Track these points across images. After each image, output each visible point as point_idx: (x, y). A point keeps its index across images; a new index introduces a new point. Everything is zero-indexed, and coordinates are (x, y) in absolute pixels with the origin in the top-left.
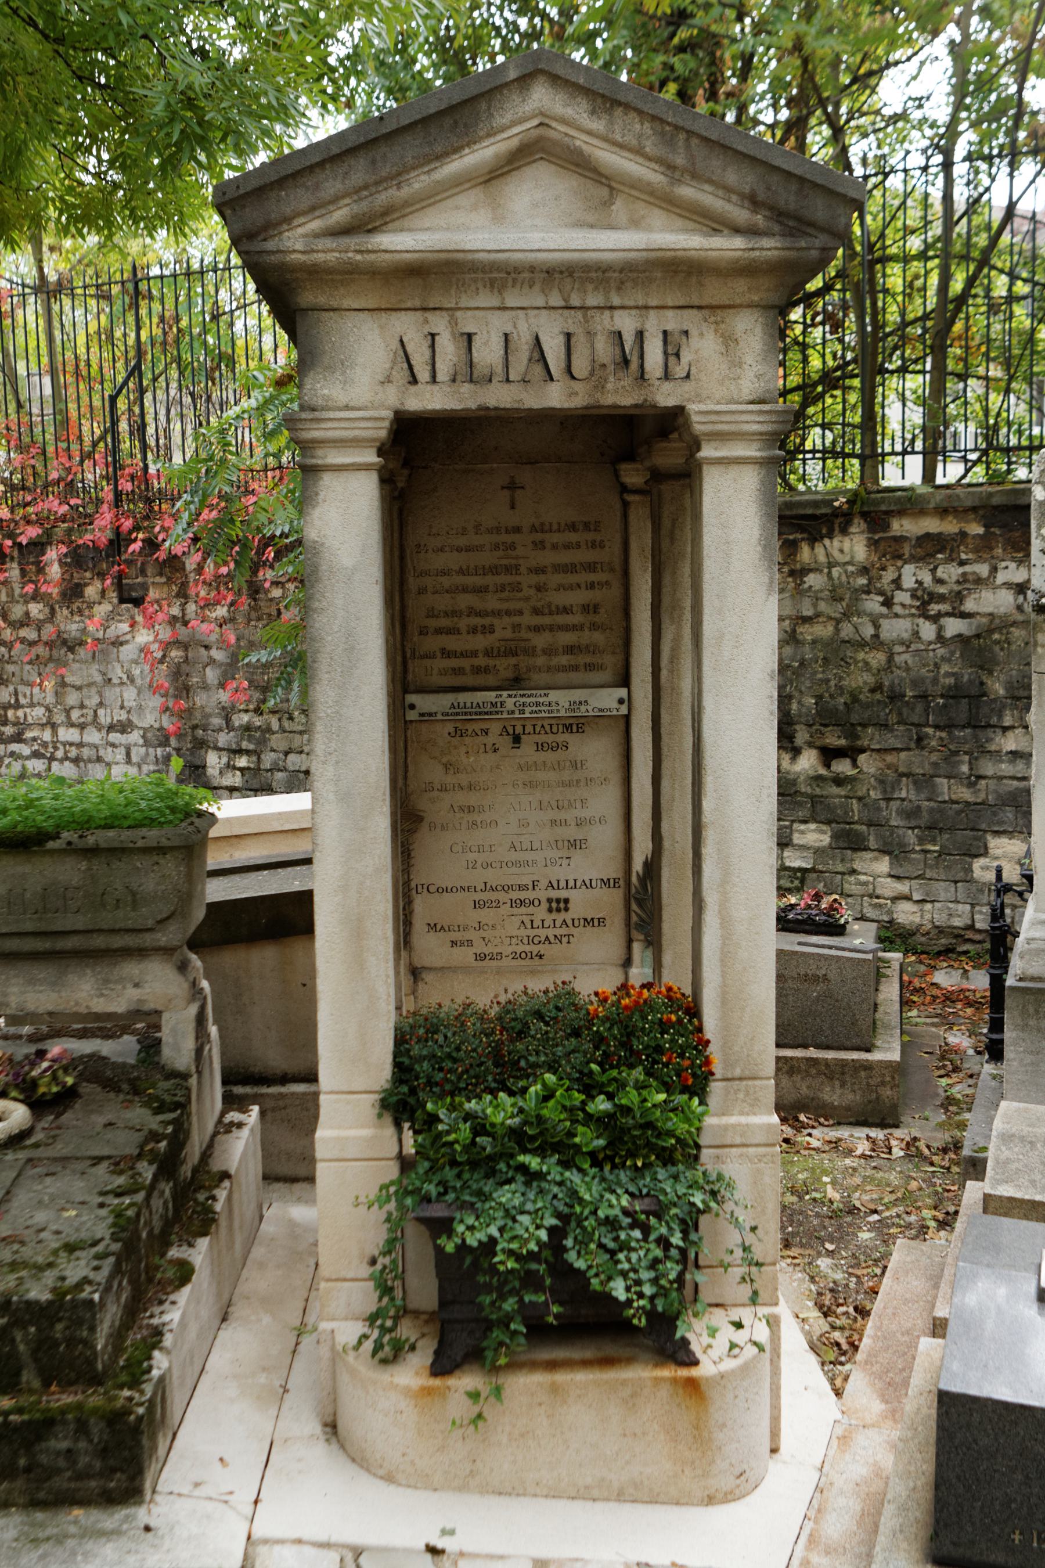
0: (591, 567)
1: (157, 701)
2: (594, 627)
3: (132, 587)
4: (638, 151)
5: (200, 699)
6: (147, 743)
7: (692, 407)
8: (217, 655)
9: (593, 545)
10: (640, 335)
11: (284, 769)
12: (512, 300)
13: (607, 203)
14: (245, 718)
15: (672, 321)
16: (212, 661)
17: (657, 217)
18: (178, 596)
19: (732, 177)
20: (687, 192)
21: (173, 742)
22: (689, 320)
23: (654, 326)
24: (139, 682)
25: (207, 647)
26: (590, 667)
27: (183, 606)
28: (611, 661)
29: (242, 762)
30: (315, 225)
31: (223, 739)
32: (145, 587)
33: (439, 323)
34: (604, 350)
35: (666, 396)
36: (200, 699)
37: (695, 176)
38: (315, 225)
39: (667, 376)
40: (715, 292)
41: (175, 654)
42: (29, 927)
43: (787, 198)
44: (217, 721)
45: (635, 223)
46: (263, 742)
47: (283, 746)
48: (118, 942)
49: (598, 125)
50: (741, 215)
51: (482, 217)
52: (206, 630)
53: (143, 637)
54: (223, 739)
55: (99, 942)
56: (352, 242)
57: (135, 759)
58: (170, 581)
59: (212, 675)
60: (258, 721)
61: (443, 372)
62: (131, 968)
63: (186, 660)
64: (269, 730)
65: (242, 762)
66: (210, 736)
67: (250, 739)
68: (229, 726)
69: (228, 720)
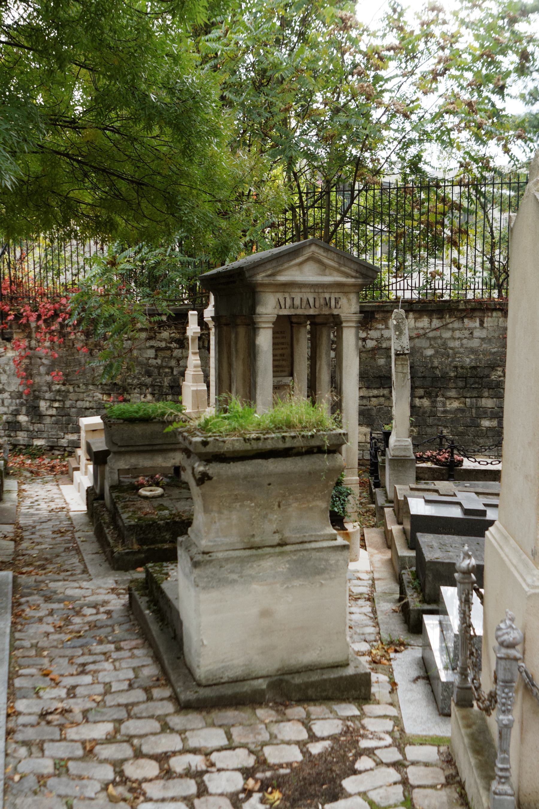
0: (282, 344)
1: (19, 381)
2: (283, 360)
3: (6, 334)
4: (333, 260)
5: (37, 379)
6: (12, 398)
7: (342, 315)
8: (45, 361)
9: (283, 338)
10: (330, 298)
11: (75, 407)
12: (303, 290)
13: (325, 270)
14: (58, 387)
15: (337, 295)
16: (43, 364)
17: (335, 273)
18: (27, 337)
19: (352, 266)
20: (343, 269)
21: (24, 397)
22: (340, 295)
23: (333, 296)
24: (8, 372)
25: (40, 358)
26: (282, 371)
27: (29, 341)
28: (288, 369)
29: (56, 405)
30: (264, 274)
31: (48, 395)
32: (11, 333)
33: (287, 295)
34: (322, 301)
35: (335, 312)
36: (37, 379)
37: (345, 266)
38: (264, 274)
39: (336, 307)
40: (346, 289)
41: (26, 361)
42: (147, 443)
43: (364, 271)
44: (45, 388)
45: (330, 275)
46: (66, 396)
47: (75, 398)
48: (170, 447)
49: (325, 254)
50: (354, 274)
51: (298, 273)
52: (42, 352)
53: (10, 354)
54: (48, 395)
55: (165, 447)
56: (272, 278)
57: (6, 404)
58: (23, 331)
59: (42, 370)
60: (63, 388)
61: (287, 306)
62: (171, 454)
63: (31, 363)
64: (68, 392)
65: (56, 405)
66: (42, 394)
67: (60, 395)
68: (50, 390)
69: (50, 388)
